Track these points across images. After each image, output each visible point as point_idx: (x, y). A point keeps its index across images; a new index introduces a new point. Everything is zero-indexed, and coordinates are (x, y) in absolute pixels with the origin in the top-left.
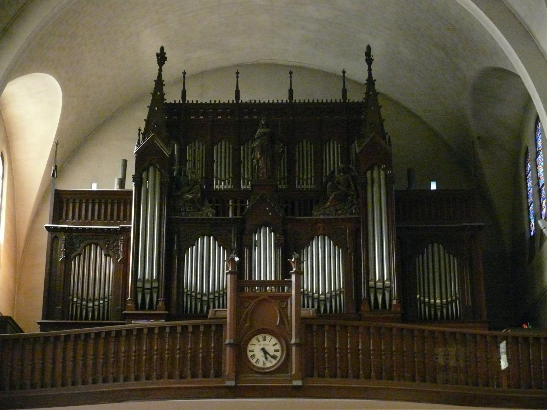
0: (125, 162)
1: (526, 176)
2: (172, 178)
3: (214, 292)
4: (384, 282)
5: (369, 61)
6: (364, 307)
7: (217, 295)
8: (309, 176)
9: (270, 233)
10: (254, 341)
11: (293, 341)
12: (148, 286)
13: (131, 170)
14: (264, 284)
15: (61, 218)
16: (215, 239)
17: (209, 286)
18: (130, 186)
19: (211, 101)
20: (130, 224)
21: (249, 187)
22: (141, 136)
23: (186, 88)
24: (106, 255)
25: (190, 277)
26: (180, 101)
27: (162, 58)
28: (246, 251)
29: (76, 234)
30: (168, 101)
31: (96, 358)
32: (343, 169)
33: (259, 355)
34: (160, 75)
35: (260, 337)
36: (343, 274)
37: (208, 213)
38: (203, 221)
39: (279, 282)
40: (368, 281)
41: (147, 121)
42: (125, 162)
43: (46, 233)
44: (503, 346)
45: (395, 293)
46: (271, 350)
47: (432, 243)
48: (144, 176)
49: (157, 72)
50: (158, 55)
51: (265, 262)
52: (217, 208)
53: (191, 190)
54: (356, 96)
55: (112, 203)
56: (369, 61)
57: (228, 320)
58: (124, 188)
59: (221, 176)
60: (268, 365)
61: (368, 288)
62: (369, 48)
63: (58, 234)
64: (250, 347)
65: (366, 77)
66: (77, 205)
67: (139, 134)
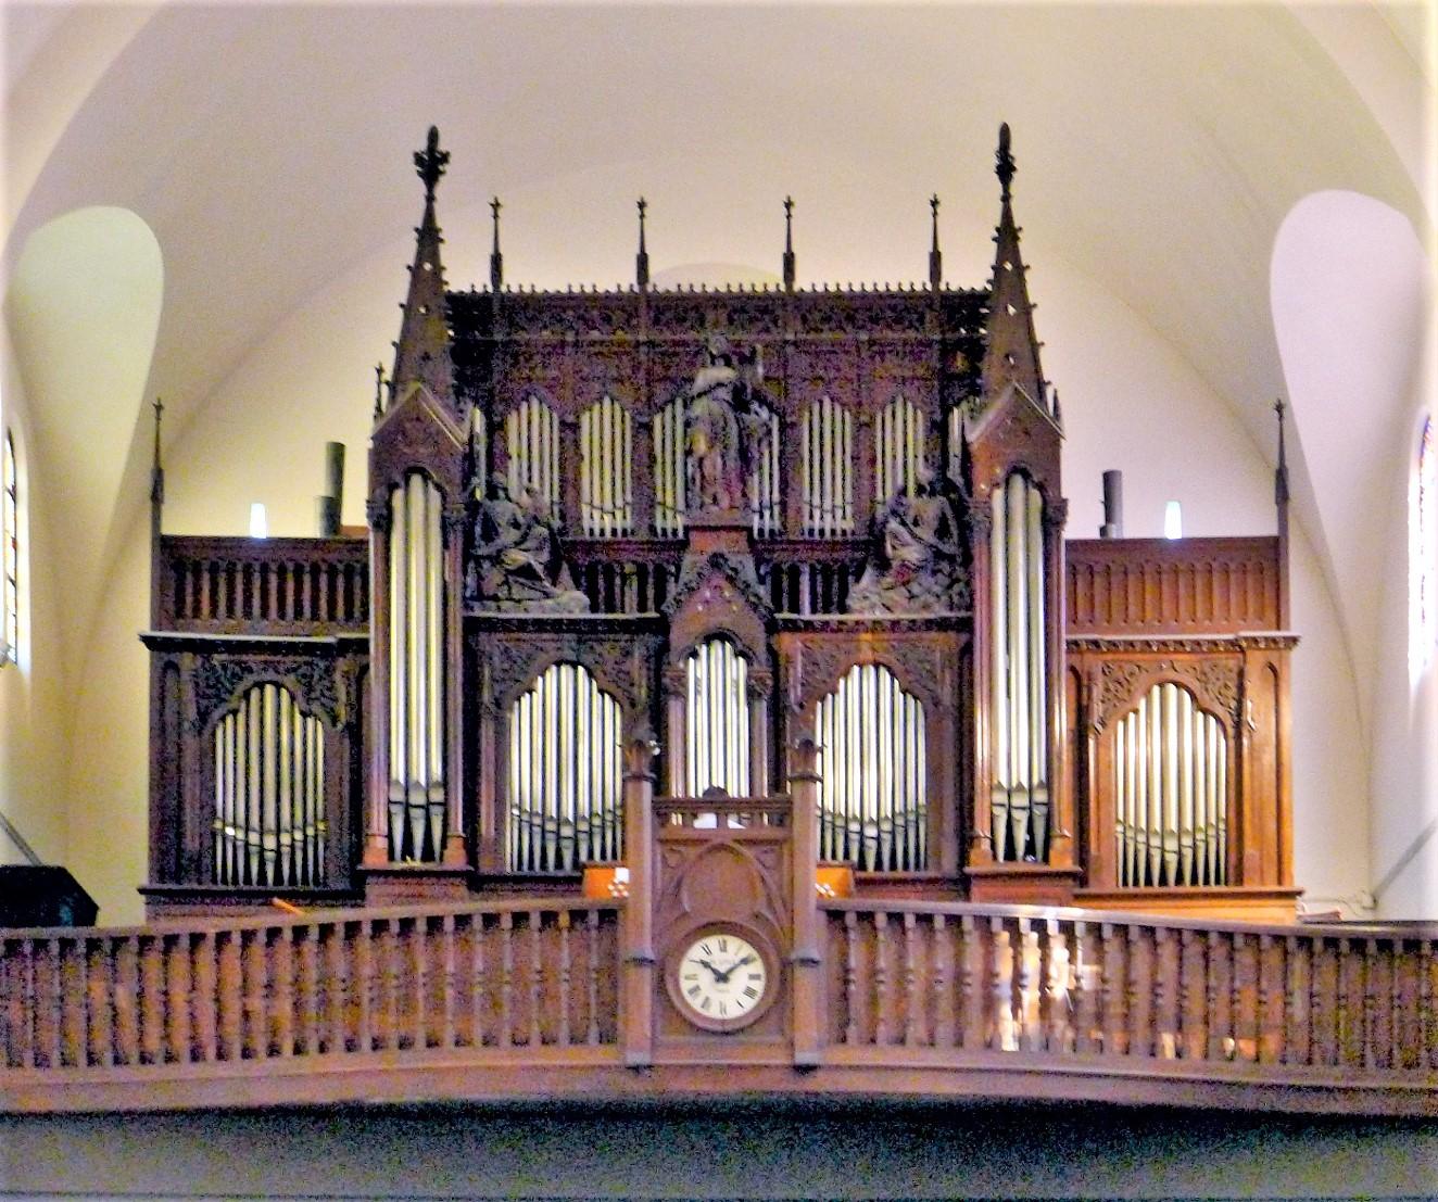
0: (337, 453)
2: (473, 506)
5: (1006, 170)
7: (584, 827)
8: (839, 501)
15: (180, 613)
19: (619, 286)
20: (366, 630)
22: (385, 389)
24: (305, 715)
26: (924, 284)
29: (224, 657)
31: (300, 990)
32: (930, 483)
37: (570, 602)
38: (557, 626)
41: (401, 348)
42: (337, 453)
43: (144, 653)
49: (423, 204)
50: (419, 159)
51: (717, 736)
52: (591, 592)
53: (524, 538)
54: (969, 272)
55: (334, 571)
56: (1006, 170)
58: (366, 528)
59: (602, 501)
62: (1005, 133)
63: (174, 657)
66: (239, 578)
67: (379, 383)
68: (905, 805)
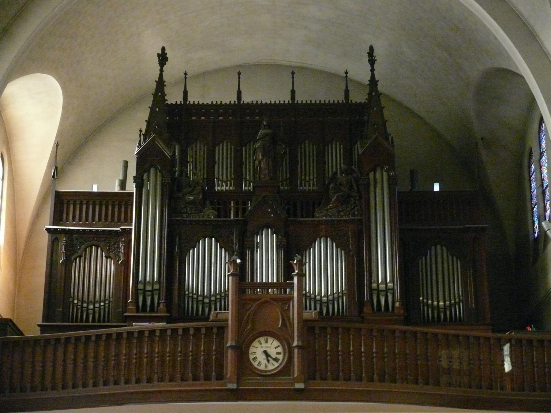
0: (126, 163)
1: (530, 177)
2: (173, 179)
3: (215, 294)
4: (386, 284)
5: (372, 61)
6: (367, 310)
7: (218, 297)
8: (312, 177)
9: (272, 234)
10: (256, 343)
11: (295, 344)
12: (149, 288)
13: (132, 171)
14: (266, 286)
15: (61, 220)
16: (217, 241)
17: (210, 288)
18: (131, 187)
19: (212, 102)
20: (131, 225)
21: (251, 188)
22: (142, 137)
23: (187, 89)
24: (107, 257)
25: (191, 279)
26: (181, 102)
27: (163, 58)
28: (248, 253)
29: (76, 236)
30: (169, 102)
31: (97, 361)
32: (346, 170)
33: (261, 358)
34: (161, 76)
35: (262, 339)
36: (345, 276)
37: (210, 214)
38: (204, 223)
39: (281, 284)
40: (371, 283)
41: (148, 122)
42: (126, 163)
43: (46, 234)
44: (506, 349)
45: (398, 295)
46: (273, 352)
47: (436, 245)
48: (145, 177)
49: (158, 72)
50: (159, 55)
51: (267, 264)
52: (218, 210)
53: (192, 191)
54: (359, 97)
55: (113, 204)
56: (372, 61)
57: (230, 322)
58: (125, 190)
59: (223, 177)
60: (270, 367)
61: (371, 290)
62: (371, 48)
63: (58, 236)
64: (252, 350)
65: (369, 78)
66: (78, 206)
67: (140, 135)
68: (100, 298)
